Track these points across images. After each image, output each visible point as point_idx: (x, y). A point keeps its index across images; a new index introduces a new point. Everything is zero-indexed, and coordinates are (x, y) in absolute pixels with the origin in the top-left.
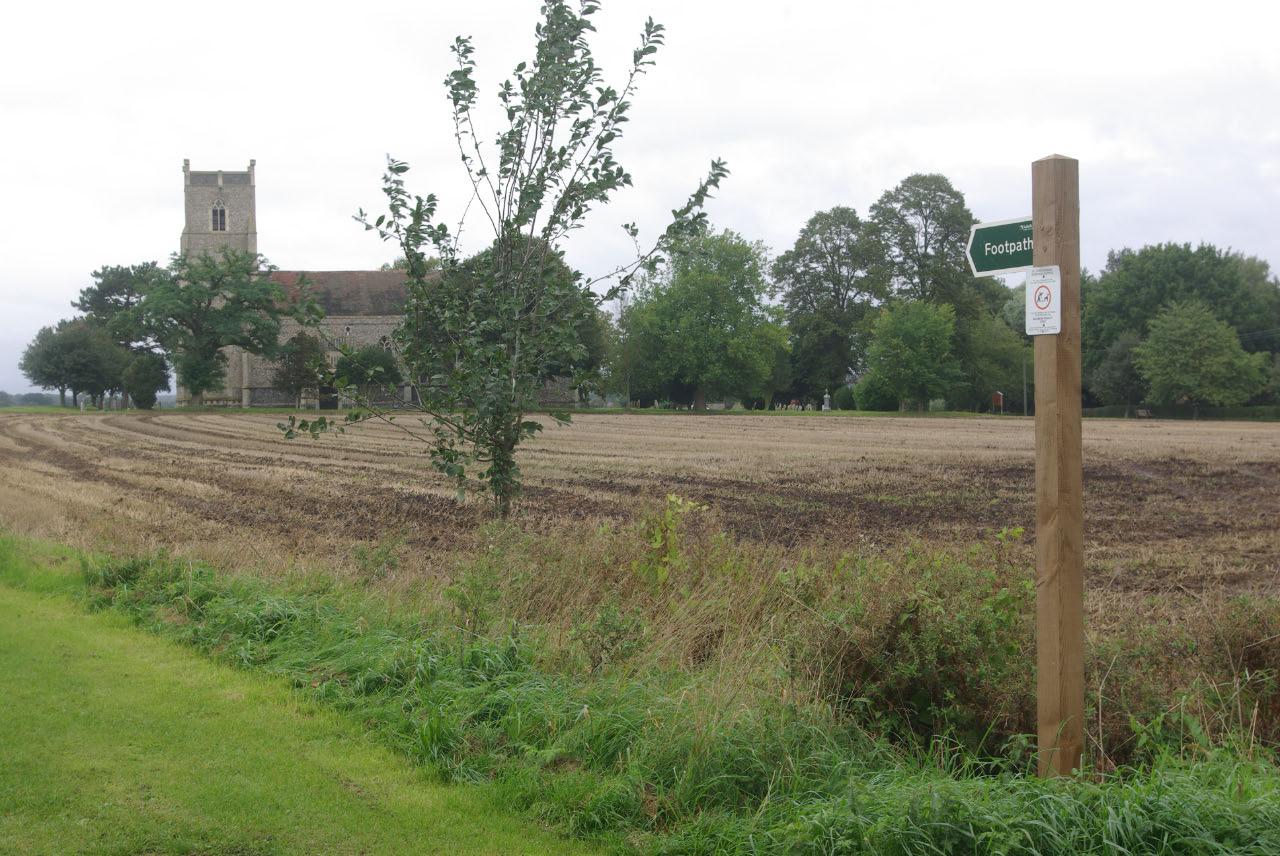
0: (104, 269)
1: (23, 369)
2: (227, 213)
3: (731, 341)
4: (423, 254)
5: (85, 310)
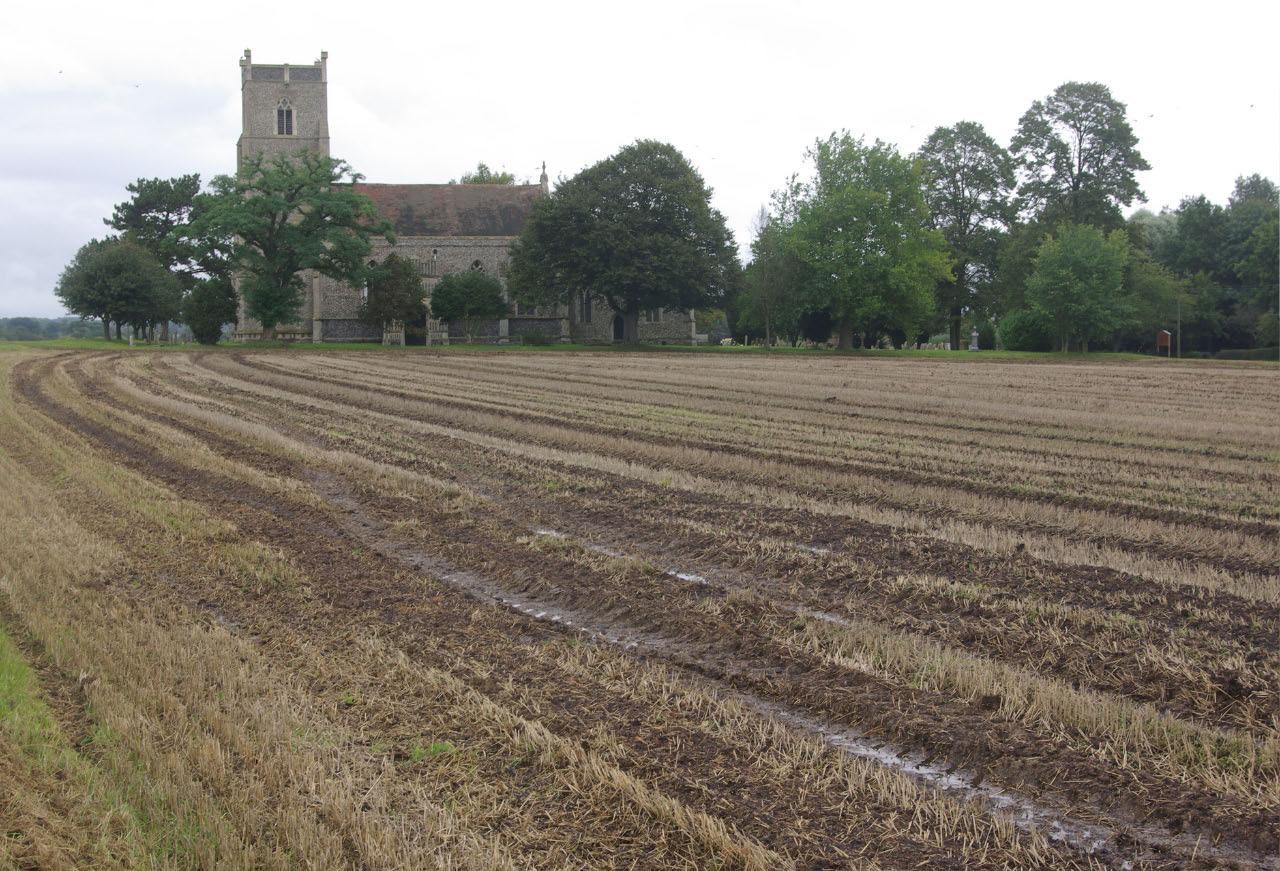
0: (140, 182)
1: (60, 295)
2: (294, 114)
3: (893, 270)
4: (866, 148)
5: (120, 228)
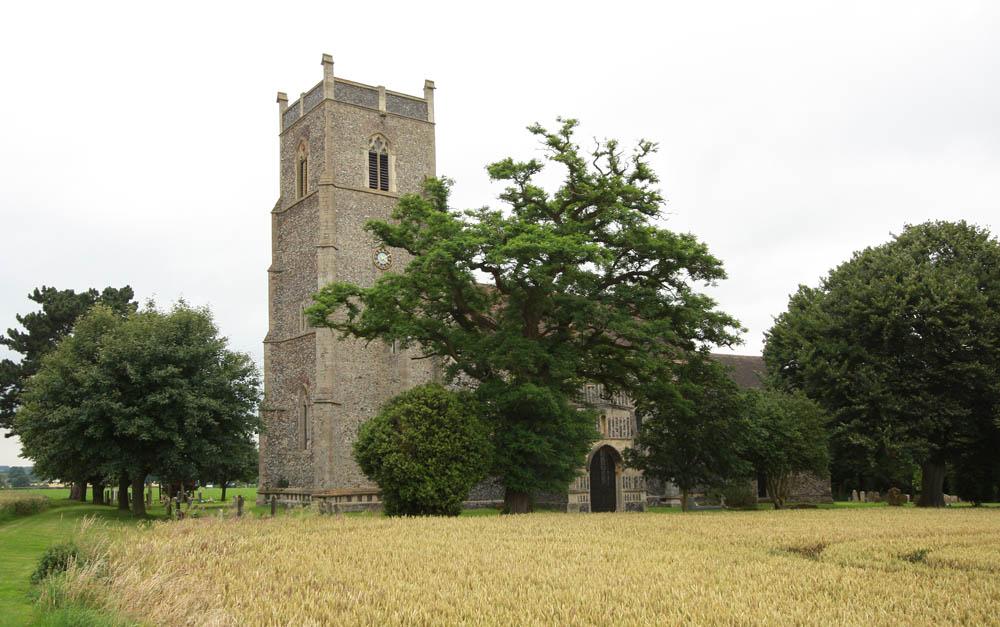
2: (392, 161)
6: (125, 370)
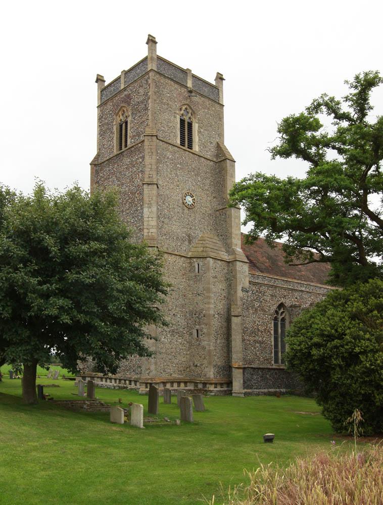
2: (195, 127)
6: (41, 241)
